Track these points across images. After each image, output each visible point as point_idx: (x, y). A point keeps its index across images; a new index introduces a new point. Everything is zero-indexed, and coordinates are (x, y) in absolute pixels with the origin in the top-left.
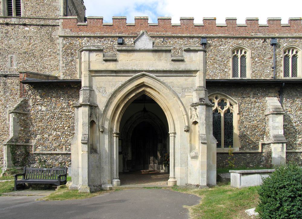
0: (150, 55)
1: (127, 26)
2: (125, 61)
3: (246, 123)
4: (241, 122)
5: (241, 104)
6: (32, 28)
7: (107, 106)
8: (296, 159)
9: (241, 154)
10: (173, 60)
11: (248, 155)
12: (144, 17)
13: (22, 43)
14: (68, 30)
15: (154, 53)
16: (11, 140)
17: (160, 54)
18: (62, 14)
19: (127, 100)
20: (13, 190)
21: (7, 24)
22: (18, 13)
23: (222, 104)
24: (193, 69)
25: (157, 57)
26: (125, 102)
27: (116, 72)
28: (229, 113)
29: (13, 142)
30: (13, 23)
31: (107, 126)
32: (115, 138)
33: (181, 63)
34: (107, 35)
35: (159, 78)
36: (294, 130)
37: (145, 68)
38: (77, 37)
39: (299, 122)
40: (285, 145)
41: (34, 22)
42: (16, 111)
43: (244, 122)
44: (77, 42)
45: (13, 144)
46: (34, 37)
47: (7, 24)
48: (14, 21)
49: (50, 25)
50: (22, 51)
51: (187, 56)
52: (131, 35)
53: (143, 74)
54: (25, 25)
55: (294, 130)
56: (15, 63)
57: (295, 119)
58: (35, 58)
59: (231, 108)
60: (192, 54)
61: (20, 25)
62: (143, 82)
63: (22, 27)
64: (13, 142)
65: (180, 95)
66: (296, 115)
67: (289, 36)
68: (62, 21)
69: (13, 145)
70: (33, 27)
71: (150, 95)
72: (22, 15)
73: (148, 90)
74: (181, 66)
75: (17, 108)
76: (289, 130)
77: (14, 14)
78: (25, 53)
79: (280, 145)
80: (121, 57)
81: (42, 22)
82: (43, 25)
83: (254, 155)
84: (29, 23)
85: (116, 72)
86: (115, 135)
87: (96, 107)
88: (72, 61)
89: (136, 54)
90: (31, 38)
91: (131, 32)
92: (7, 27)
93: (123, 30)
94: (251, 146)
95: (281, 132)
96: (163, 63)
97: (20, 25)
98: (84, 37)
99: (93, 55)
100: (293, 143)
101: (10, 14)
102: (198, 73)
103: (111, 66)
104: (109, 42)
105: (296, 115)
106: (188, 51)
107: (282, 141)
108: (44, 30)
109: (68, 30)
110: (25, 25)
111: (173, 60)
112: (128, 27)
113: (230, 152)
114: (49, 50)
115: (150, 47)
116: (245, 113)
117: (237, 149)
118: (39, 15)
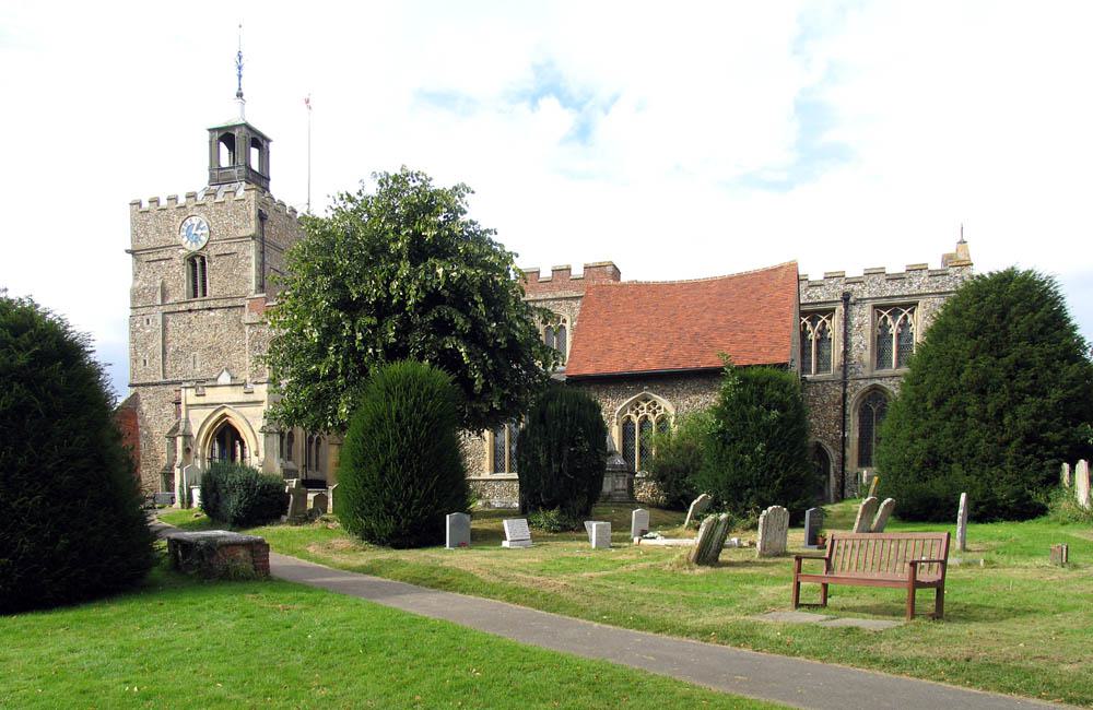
0: (229, 388)
6: (218, 313)
14: (255, 314)
16: (165, 468)
18: (253, 285)
21: (190, 311)
37: (226, 401)
41: (220, 304)
47: (190, 311)
48: (197, 305)
50: (206, 345)
54: (210, 309)
56: (198, 364)
60: (260, 386)
61: (203, 309)
63: (206, 312)
67: (550, 297)
72: (212, 290)
74: (251, 398)
75: (170, 433)
77: (200, 294)
78: (210, 348)
80: (208, 391)
81: (230, 304)
90: (216, 326)
92: (190, 315)
96: (238, 395)
97: (203, 309)
99: (189, 390)
103: (201, 400)
106: (256, 383)
109: (255, 314)
110: (210, 309)
115: (228, 381)
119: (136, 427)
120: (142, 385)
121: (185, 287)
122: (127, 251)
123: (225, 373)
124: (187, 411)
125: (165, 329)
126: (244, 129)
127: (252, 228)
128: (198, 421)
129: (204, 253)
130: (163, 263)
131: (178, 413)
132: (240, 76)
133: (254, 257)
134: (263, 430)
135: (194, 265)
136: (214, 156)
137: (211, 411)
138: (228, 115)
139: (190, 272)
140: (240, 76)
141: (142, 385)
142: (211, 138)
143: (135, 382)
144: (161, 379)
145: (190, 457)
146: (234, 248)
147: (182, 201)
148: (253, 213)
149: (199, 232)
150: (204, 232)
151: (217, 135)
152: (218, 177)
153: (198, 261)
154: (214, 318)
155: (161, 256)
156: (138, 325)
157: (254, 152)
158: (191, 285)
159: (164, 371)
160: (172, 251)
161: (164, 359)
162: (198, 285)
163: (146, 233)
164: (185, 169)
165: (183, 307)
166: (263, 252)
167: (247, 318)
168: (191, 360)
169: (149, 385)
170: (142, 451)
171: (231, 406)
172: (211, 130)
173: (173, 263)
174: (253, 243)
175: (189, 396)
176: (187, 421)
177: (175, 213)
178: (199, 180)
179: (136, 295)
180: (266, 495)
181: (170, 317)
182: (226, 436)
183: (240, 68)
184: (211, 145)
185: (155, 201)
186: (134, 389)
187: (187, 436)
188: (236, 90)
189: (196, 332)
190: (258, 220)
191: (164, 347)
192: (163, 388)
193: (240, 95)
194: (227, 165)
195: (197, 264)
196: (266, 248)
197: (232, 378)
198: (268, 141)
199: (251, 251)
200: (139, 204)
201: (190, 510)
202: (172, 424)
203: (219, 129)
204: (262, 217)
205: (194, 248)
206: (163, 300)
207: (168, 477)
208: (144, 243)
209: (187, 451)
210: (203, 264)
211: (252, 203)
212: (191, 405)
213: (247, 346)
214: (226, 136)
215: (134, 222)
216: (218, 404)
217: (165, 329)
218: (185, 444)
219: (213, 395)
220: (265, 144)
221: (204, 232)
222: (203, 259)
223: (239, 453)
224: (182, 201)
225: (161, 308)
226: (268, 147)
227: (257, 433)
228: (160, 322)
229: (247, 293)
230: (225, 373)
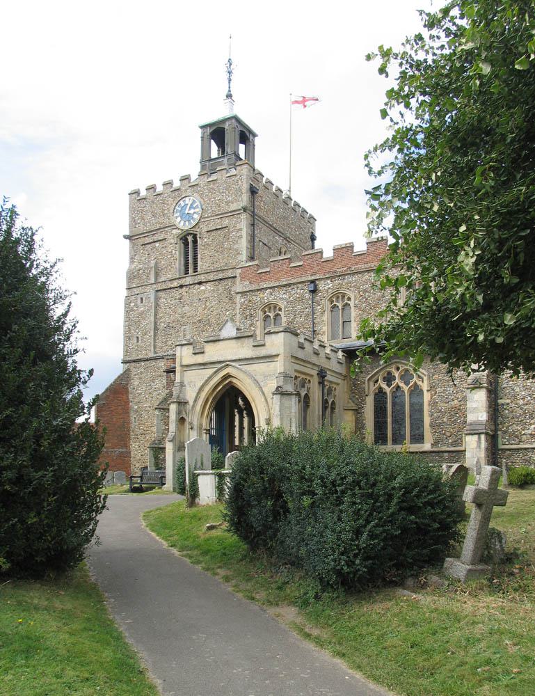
0: (234, 341)
1: (323, 262)
2: (213, 352)
3: (442, 406)
4: (433, 404)
5: (433, 375)
6: (209, 287)
7: (195, 401)
8: (526, 460)
9: (434, 454)
10: (254, 346)
11: (446, 454)
12: (346, 244)
13: (196, 310)
14: (247, 283)
15: (237, 340)
16: (154, 443)
17: (243, 339)
18: (244, 256)
19: (215, 393)
20: (128, 492)
21: (181, 286)
22: (195, 269)
23: (406, 377)
24: (274, 354)
25: (239, 344)
26: (213, 395)
27: (204, 365)
28: (416, 391)
29: (156, 444)
30: (188, 283)
31: (195, 423)
32: (205, 435)
33: (262, 348)
34: (295, 281)
35: (241, 367)
36: (521, 412)
37: (229, 358)
38: (258, 290)
39: (529, 398)
40: (483, 437)
41: (211, 278)
42: (160, 406)
43: (437, 403)
44: (257, 298)
45: (156, 446)
46: (211, 298)
47: (181, 286)
48: (188, 280)
49: (230, 278)
51: (269, 339)
52: (327, 276)
53: (225, 364)
55: (521, 412)
57: (523, 393)
58: (210, 326)
59: (419, 383)
62: (228, 373)
63: (197, 286)
64: (156, 444)
65: (262, 384)
66: (524, 387)
68: (240, 271)
69: (155, 448)
70: (209, 284)
71: (236, 386)
73: (234, 381)
76: (512, 412)
77: (191, 270)
79: (476, 437)
80: (209, 348)
81: (220, 276)
82: (220, 279)
83: (454, 454)
84: (204, 280)
85: (204, 365)
86: (205, 432)
87: (186, 403)
88: (251, 325)
89: (220, 343)
91: (328, 270)
92: (181, 291)
93: (317, 269)
94: (450, 441)
95: (481, 417)
98: (267, 288)
99: (185, 348)
100: (520, 433)
101: (187, 272)
102: (279, 357)
103: (200, 359)
104: (299, 291)
105: (524, 387)
107: (477, 432)
108: (221, 287)
109: (247, 283)
110: (200, 283)
111: (254, 346)
112: (325, 264)
113: (403, 450)
114: (228, 313)
115: (234, 333)
116: (439, 389)
117: (427, 446)
118: (217, 266)
119: (127, 402)
120: (134, 361)
121: (178, 264)
122: (125, 237)
123: (457, 8)
124: (182, 372)
125: (157, 306)
126: (233, 120)
127: (245, 199)
128: (196, 386)
129: (197, 230)
130: (157, 245)
131: (171, 383)
132: (230, 80)
133: (245, 229)
134: (280, 392)
135: (186, 244)
136: (205, 150)
137: (211, 371)
138: (217, 112)
139: (182, 251)
140: (230, 80)
141: (134, 361)
142: (203, 133)
143: (128, 359)
144: (152, 355)
145: (184, 430)
146: (226, 222)
147: (177, 184)
148: (245, 187)
149: (192, 211)
150: (197, 210)
151: (209, 131)
152: (208, 166)
153: (190, 239)
154: (204, 291)
155: (156, 238)
156: (132, 304)
157: (242, 147)
158: (182, 263)
159: (155, 347)
160: (166, 232)
161: (155, 335)
162: (190, 260)
163: (143, 219)
164: (184, 157)
165: (175, 284)
166: (253, 225)
167: (239, 287)
168: (182, 334)
169: (140, 360)
170: (132, 426)
171: (233, 364)
172: (202, 127)
173: (166, 243)
174: (244, 216)
175: (185, 355)
176: (182, 385)
177: (169, 196)
178: (194, 170)
179: (132, 277)
180: (412, 510)
181: (162, 294)
182: (229, 403)
183: (230, 73)
184: (202, 140)
185: (152, 188)
186: (127, 366)
187: (182, 404)
188: (226, 92)
189: (186, 307)
190: (249, 194)
191: (155, 323)
192: (153, 363)
193: (229, 96)
194: (216, 156)
195: (189, 242)
196: (256, 221)
197: (238, 329)
198: (255, 135)
199: (243, 223)
200: (137, 192)
201: (194, 510)
202: (164, 393)
203: (210, 125)
204: (253, 191)
205: (187, 226)
206: (156, 279)
207: (158, 450)
208: (141, 228)
209: (182, 420)
210: (195, 242)
211: (244, 177)
212: (187, 366)
213: (238, 316)
214: (217, 133)
215: (133, 210)
216: (224, 362)
217: (157, 306)
218: (179, 412)
219: (213, 352)
220: (251, 138)
221: (197, 210)
222: (195, 236)
223: (237, 423)
224: (177, 184)
225: (154, 286)
226: (253, 141)
227: (269, 396)
228: (152, 300)
229: (238, 263)
230: (457, 8)
